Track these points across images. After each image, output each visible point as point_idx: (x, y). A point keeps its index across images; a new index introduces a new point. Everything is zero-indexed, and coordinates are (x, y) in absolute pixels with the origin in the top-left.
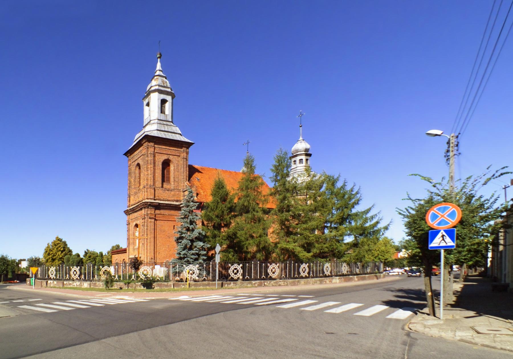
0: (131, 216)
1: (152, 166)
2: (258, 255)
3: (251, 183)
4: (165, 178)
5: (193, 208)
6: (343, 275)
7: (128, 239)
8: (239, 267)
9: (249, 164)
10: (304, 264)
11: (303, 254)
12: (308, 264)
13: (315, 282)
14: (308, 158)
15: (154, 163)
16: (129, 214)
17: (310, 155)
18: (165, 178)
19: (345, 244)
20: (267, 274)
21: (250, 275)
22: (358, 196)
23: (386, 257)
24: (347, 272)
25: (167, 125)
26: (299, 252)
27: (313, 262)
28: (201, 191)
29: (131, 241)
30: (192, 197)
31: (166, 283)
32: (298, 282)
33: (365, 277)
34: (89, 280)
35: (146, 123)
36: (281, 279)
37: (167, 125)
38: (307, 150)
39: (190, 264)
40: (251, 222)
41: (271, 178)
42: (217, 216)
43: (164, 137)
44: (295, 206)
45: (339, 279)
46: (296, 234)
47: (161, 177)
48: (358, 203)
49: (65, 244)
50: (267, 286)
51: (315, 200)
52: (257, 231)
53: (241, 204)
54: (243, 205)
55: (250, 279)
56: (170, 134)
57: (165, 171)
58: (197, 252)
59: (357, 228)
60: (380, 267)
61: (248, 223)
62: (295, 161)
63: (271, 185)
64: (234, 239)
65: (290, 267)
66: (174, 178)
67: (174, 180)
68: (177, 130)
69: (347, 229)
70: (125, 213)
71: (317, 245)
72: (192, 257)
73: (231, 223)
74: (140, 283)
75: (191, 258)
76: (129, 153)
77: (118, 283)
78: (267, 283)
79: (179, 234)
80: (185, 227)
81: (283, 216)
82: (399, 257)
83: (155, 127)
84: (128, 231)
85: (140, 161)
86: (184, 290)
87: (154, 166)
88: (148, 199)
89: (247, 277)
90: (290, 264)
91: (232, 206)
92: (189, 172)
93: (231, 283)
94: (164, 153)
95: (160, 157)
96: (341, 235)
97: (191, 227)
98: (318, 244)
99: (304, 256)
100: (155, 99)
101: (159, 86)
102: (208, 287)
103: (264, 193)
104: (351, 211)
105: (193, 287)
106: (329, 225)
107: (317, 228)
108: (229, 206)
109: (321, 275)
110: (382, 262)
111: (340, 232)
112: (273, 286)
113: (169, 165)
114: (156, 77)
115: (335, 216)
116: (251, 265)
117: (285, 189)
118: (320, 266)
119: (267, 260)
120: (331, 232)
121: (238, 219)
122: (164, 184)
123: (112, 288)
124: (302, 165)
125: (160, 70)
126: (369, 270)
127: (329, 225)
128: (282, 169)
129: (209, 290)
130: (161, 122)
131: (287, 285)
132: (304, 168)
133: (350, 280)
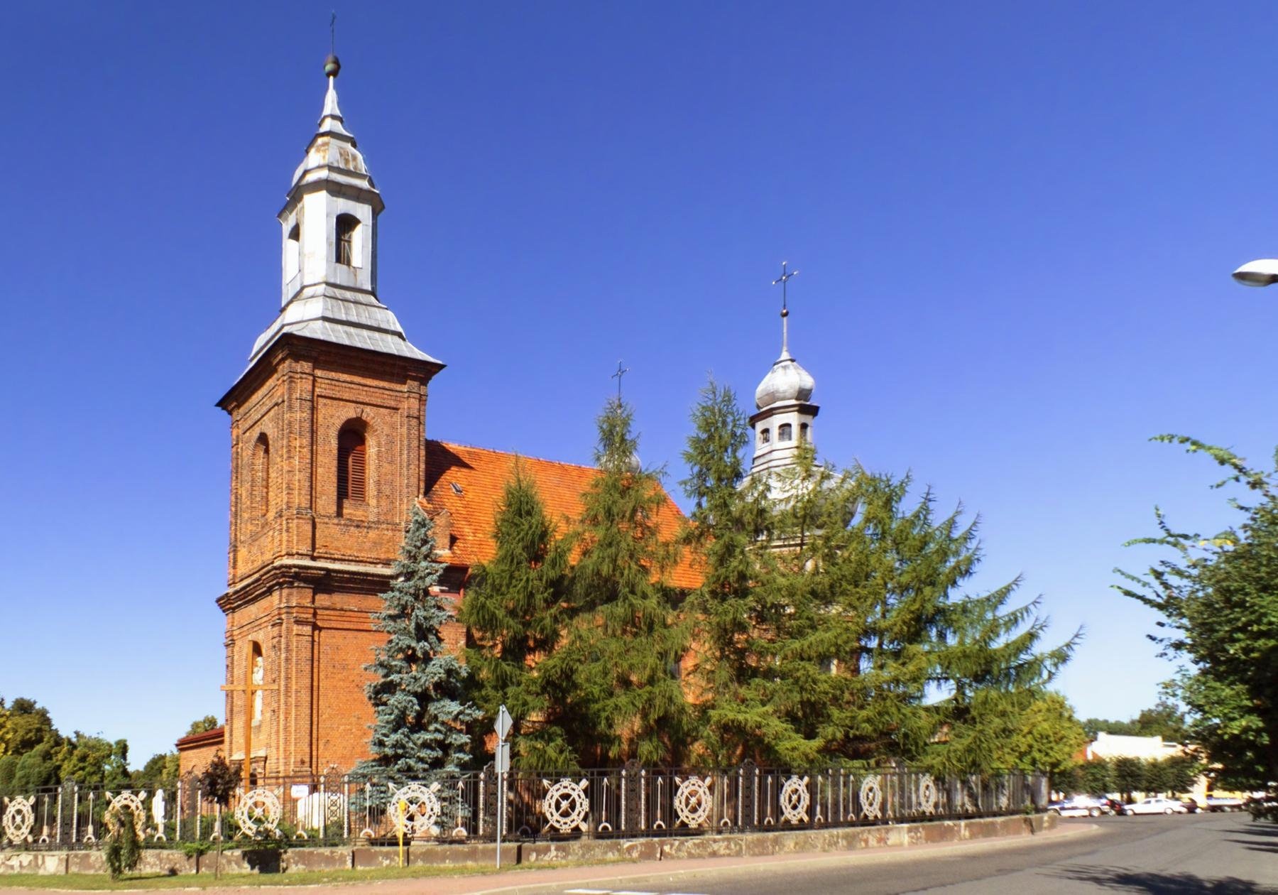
0: (237, 615)
1: (306, 441)
2: (645, 748)
3: (622, 500)
4: (348, 486)
5: (428, 580)
6: (923, 818)
7: (230, 695)
8: (577, 790)
9: (615, 438)
10: (795, 778)
11: (794, 745)
12: (806, 779)
13: (833, 843)
14: (808, 419)
15: (313, 432)
16: (234, 610)
17: (812, 411)
18: (348, 486)
19: (927, 709)
20: (671, 814)
21: (614, 817)
22: (972, 545)
23: (1056, 755)
24: (936, 806)
25: (355, 302)
26: (776, 737)
27: (824, 772)
28: (467, 530)
29: (239, 702)
30: (425, 542)
31: (326, 851)
32: (776, 841)
33: (993, 824)
34: (66, 843)
35: (290, 297)
36: (720, 832)
37: (355, 302)
38: (803, 394)
39: (415, 778)
40: (624, 632)
41: (685, 483)
42: (512, 613)
43: (346, 342)
44: (764, 578)
45: (910, 830)
46: (769, 674)
47: (335, 480)
48: (968, 572)
49: (44, 718)
50: (673, 857)
51: (830, 558)
52: (642, 661)
53: (589, 571)
54: (598, 573)
55: (617, 834)
56: (365, 333)
57: (350, 460)
58: (440, 737)
59: (965, 655)
60: (1040, 791)
61: (614, 635)
62: (766, 431)
63: (688, 506)
64: (565, 692)
65: (748, 788)
66: (378, 483)
67: (379, 491)
68: (389, 319)
69: (933, 657)
70: (221, 606)
71: (835, 713)
72: (422, 755)
73: (556, 634)
74: (238, 853)
75: (421, 760)
76: (234, 399)
77: (165, 853)
78: (671, 845)
79: (381, 672)
80: (401, 650)
81: (726, 613)
82: (1090, 757)
83: (315, 308)
84: (230, 667)
85: (271, 433)
86: (385, 876)
87: (313, 442)
88: (289, 555)
89: (611, 822)
90: (749, 778)
91: (562, 577)
92: (427, 463)
93: (548, 850)
94: (346, 396)
95: (331, 411)
96: (915, 680)
97: (420, 647)
98: (840, 707)
99: (794, 749)
100: (317, 212)
101: (331, 168)
102: (470, 863)
103: (665, 535)
104: (946, 596)
105: (420, 863)
106: (874, 644)
107: (837, 655)
108: (552, 574)
109: (851, 816)
110: (1044, 773)
111: (911, 667)
112: (691, 856)
113: (362, 441)
114: (320, 140)
115: (894, 614)
116: (620, 780)
117: (734, 522)
118: (845, 785)
119: (675, 763)
120: (882, 667)
121: (582, 623)
122: (347, 503)
123: (136, 873)
124: (787, 444)
125: (334, 117)
126: (1004, 802)
127: (874, 644)
128: (719, 454)
129: (472, 873)
130: (338, 292)
131: (738, 854)
132: (796, 452)
133: (945, 835)
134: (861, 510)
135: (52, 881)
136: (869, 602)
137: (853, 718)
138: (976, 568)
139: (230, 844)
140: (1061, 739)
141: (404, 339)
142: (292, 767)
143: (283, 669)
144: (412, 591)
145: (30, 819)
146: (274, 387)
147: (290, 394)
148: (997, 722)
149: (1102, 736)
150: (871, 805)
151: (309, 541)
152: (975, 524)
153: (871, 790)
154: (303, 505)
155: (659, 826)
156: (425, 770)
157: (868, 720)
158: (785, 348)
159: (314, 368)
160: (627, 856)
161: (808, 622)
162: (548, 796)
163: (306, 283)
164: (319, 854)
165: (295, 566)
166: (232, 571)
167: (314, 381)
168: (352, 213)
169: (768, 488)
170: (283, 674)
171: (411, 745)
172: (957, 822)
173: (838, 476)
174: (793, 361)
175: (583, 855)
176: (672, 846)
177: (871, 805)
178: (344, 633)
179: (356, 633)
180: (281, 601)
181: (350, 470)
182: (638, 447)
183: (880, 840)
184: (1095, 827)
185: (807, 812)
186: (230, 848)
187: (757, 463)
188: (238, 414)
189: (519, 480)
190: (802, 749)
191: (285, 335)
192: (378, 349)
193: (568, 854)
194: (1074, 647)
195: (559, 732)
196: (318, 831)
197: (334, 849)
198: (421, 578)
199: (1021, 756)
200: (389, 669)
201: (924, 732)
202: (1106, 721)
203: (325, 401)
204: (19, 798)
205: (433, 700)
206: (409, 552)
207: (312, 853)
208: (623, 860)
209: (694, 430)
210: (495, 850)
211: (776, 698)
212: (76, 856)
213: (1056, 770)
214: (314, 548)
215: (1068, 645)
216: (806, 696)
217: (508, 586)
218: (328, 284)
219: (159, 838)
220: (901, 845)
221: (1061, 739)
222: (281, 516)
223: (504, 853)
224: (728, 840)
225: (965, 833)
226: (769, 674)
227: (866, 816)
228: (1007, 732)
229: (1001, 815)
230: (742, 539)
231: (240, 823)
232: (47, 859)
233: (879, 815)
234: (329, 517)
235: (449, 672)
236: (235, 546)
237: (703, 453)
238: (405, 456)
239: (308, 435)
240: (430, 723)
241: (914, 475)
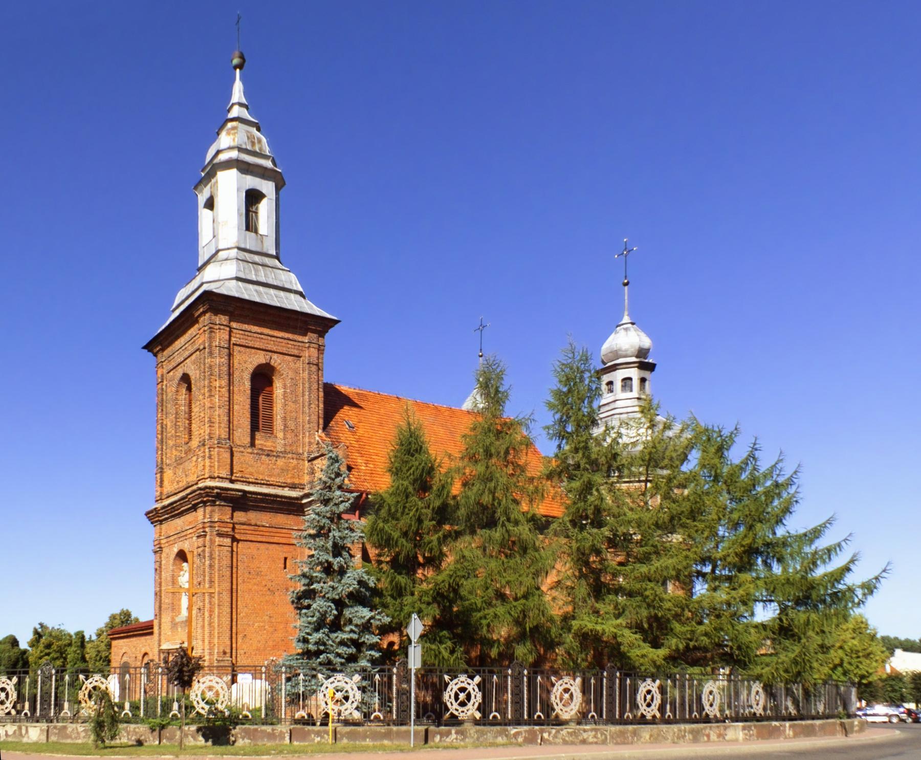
0: (164, 526)
1: (224, 382)
2: (521, 651)
3: (495, 439)
4: (259, 420)
6: (754, 718)
9: (493, 391)
14: (646, 374)
15: (230, 374)
16: (161, 522)
17: (651, 367)
18: (259, 420)
20: (548, 708)
22: (792, 490)
23: (864, 667)
24: (765, 709)
25: (263, 265)
27: (671, 676)
29: (166, 600)
31: (268, 729)
32: (635, 733)
33: (812, 725)
35: (206, 258)
37: (263, 265)
38: (642, 353)
41: (548, 428)
43: (257, 299)
44: (615, 510)
45: (744, 728)
46: (618, 590)
47: (248, 415)
50: (550, 743)
56: (272, 291)
57: (261, 399)
58: (355, 636)
62: (610, 383)
64: (452, 602)
66: (285, 419)
67: (285, 426)
71: (677, 627)
72: (340, 651)
73: (442, 555)
74: (193, 728)
76: (159, 343)
77: (132, 726)
78: (549, 733)
80: (321, 563)
84: (158, 570)
85: (194, 374)
87: (230, 383)
92: (325, 403)
93: (449, 733)
95: (245, 357)
99: (643, 656)
100: (229, 187)
101: (240, 149)
102: (386, 742)
105: (345, 741)
106: (708, 569)
107: (677, 578)
110: (853, 684)
111: (741, 592)
112: (565, 742)
113: (270, 383)
114: (230, 125)
117: (588, 461)
120: (715, 589)
123: (113, 743)
124: (629, 395)
125: (241, 105)
127: (708, 569)
128: (576, 401)
130: (248, 256)
131: (604, 742)
133: (773, 733)
134: (695, 456)
135: (36, 747)
136: (706, 534)
137: (693, 632)
138: (796, 508)
139: (187, 721)
140: (869, 654)
141: (304, 297)
142: (216, 657)
143: (207, 574)
144: (328, 515)
145: (14, 696)
146: (195, 336)
147: (211, 343)
148: (818, 640)
149: (899, 652)
150: (711, 705)
151: (228, 467)
152: (795, 472)
153: (711, 693)
154: (223, 436)
155: (539, 717)
156: (342, 664)
157: (706, 634)
158: (626, 313)
159: (230, 321)
160: (514, 740)
161: (653, 549)
162: (449, 689)
163: (220, 247)
164: (262, 731)
165: (217, 488)
166: (159, 489)
167: (230, 332)
168: (258, 188)
169: (620, 435)
170: (207, 578)
171: (330, 642)
172: (783, 723)
173: (677, 427)
174: (633, 324)
175: (478, 739)
176: (550, 733)
177: (711, 705)
178: (258, 545)
179: (267, 545)
180: (204, 517)
181: (261, 407)
182: (510, 397)
183: (719, 735)
184: (897, 732)
185: (659, 710)
186: (187, 724)
187: (602, 410)
188: (163, 356)
189: (409, 424)
190: (650, 656)
191: (206, 293)
192: (283, 306)
193: (465, 737)
194: (881, 580)
195: (447, 635)
196: (260, 710)
197: (274, 727)
198: (336, 504)
199: (834, 668)
200: (312, 580)
201: (753, 646)
202: (896, 638)
203: (239, 348)
204: (649, 681)
205: (348, 606)
206: (325, 483)
207: (256, 730)
208: (511, 744)
209: (554, 383)
210: (409, 732)
211: (627, 612)
212: (55, 727)
213: (864, 681)
214: (232, 473)
215: (876, 578)
216: (653, 612)
217: (403, 513)
218: (239, 249)
219: (126, 714)
220: (737, 740)
221: (869, 654)
222: (204, 445)
223: (416, 733)
224: (596, 730)
225: (789, 732)
226: (618, 590)
227: (707, 715)
228: (824, 649)
229: (819, 719)
230: (598, 478)
231: (195, 703)
232: (30, 730)
233: (718, 715)
234: (244, 447)
235: (361, 583)
236: (162, 468)
237: (564, 404)
238: (307, 397)
239: (226, 377)
240: (345, 625)
241: (761, 443)
